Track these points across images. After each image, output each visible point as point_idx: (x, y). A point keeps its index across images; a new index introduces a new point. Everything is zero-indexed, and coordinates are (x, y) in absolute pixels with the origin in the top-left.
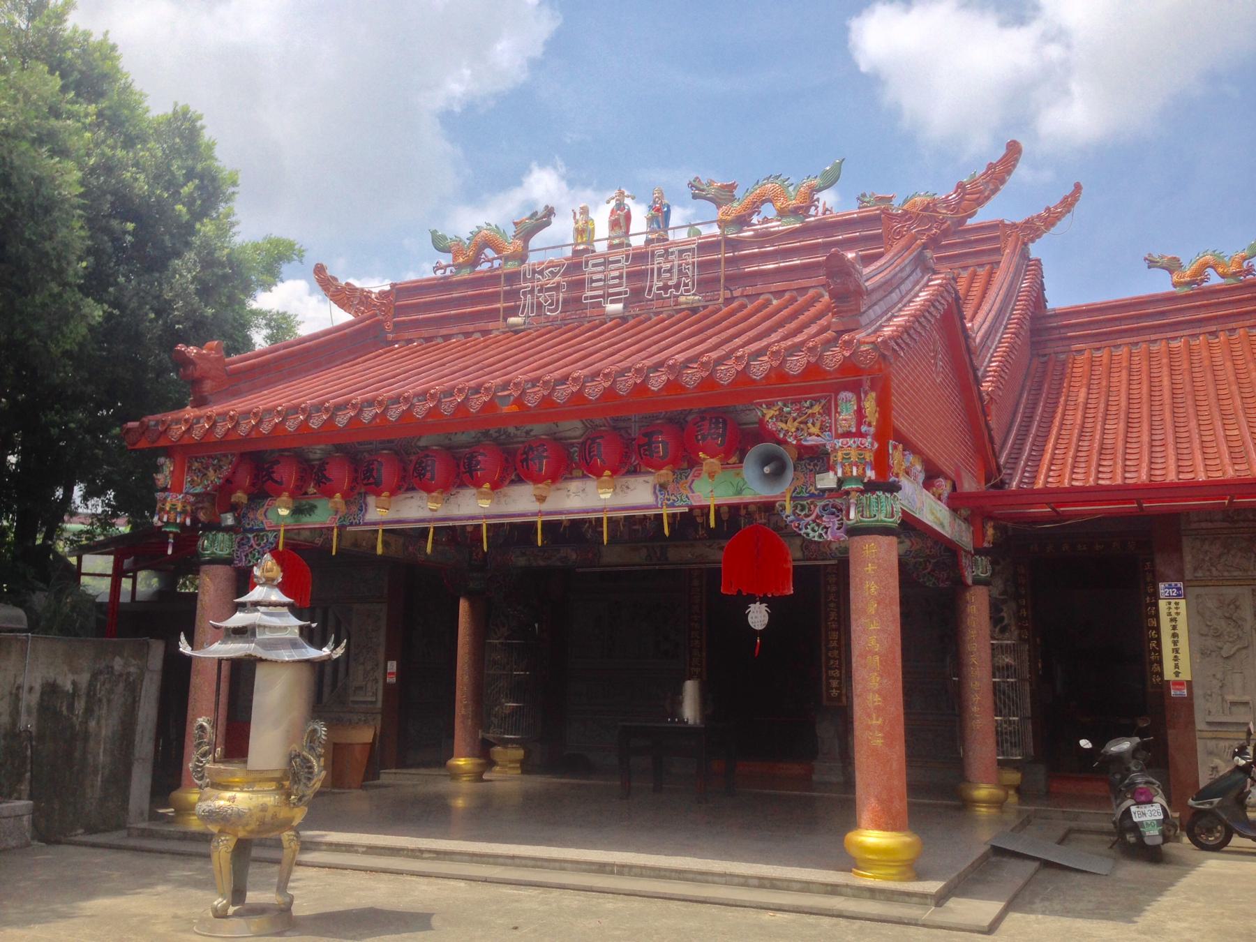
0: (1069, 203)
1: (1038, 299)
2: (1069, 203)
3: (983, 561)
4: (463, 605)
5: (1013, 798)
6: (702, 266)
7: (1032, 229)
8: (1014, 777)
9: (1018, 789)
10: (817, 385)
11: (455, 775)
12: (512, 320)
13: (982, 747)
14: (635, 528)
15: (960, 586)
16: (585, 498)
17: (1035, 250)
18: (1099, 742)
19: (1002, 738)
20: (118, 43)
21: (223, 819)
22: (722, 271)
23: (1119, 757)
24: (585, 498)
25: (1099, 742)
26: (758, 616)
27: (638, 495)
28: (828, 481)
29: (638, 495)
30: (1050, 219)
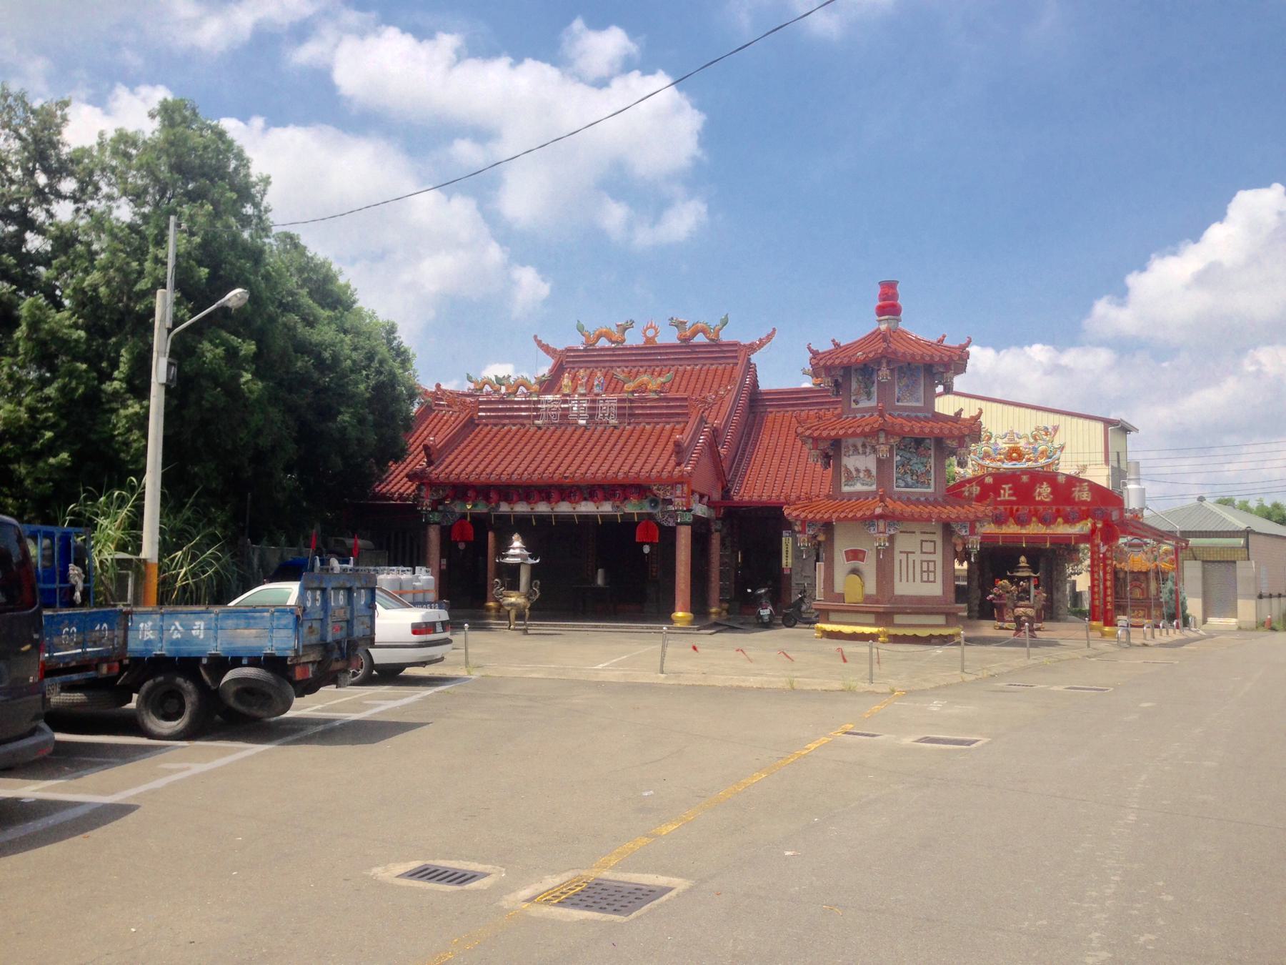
0: (769, 337)
1: (755, 383)
2: (769, 337)
3: (719, 522)
4: (491, 535)
5: (724, 613)
6: (619, 408)
7: (752, 348)
8: (726, 606)
9: (728, 611)
10: (673, 483)
11: (488, 609)
12: (537, 422)
13: (715, 594)
14: (608, 520)
15: (709, 532)
16: (587, 508)
17: (755, 358)
18: (754, 590)
19: (722, 590)
20: (393, 319)
21: (511, 604)
22: (627, 412)
23: (760, 595)
24: (587, 508)
25: (754, 590)
26: (646, 549)
27: (607, 508)
28: (671, 508)
29: (607, 508)
30: (762, 344)
